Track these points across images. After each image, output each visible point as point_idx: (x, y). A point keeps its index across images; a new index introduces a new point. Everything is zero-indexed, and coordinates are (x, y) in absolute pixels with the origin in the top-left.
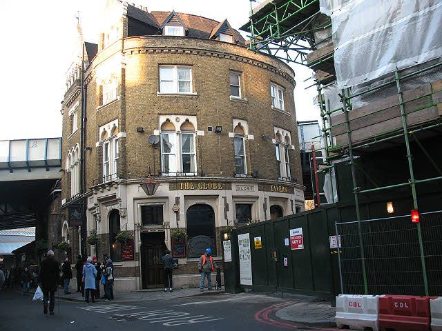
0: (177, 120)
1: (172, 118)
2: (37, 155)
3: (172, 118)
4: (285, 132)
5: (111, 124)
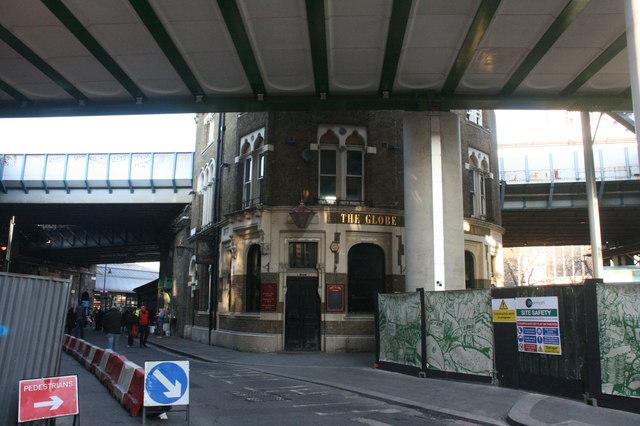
0: (343, 132)
1: (336, 131)
2: (163, 174)
3: (336, 131)
4: (483, 155)
5: (256, 135)
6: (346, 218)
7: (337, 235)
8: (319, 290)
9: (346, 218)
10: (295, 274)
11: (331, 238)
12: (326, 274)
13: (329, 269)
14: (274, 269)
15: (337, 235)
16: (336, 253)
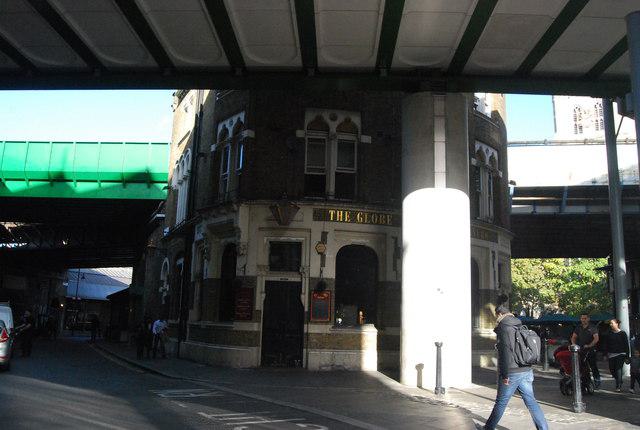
6: (335, 215)
7: (324, 235)
8: (302, 296)
9: (335, 215)
10: (276, 277)
11: (317, 237)
12: (311, 279)
13: (314, 273)
15: (324, 235)
16: (323, 256)
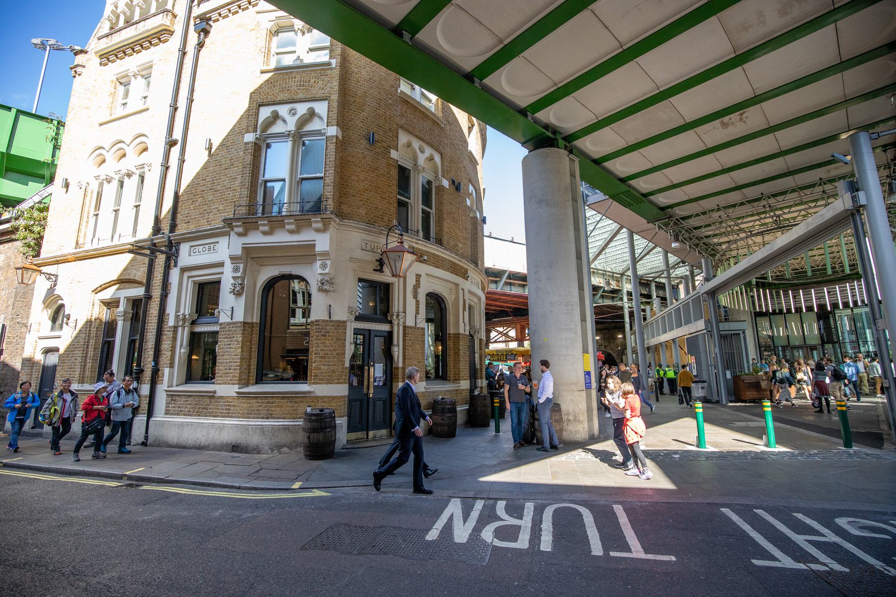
11: (411, 281)
14: (341, 314)
15: (418, 276)
